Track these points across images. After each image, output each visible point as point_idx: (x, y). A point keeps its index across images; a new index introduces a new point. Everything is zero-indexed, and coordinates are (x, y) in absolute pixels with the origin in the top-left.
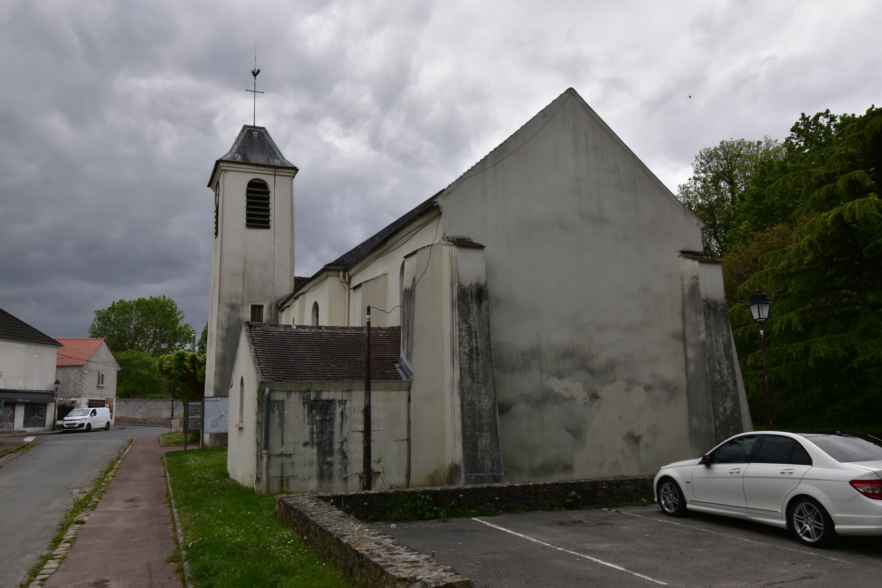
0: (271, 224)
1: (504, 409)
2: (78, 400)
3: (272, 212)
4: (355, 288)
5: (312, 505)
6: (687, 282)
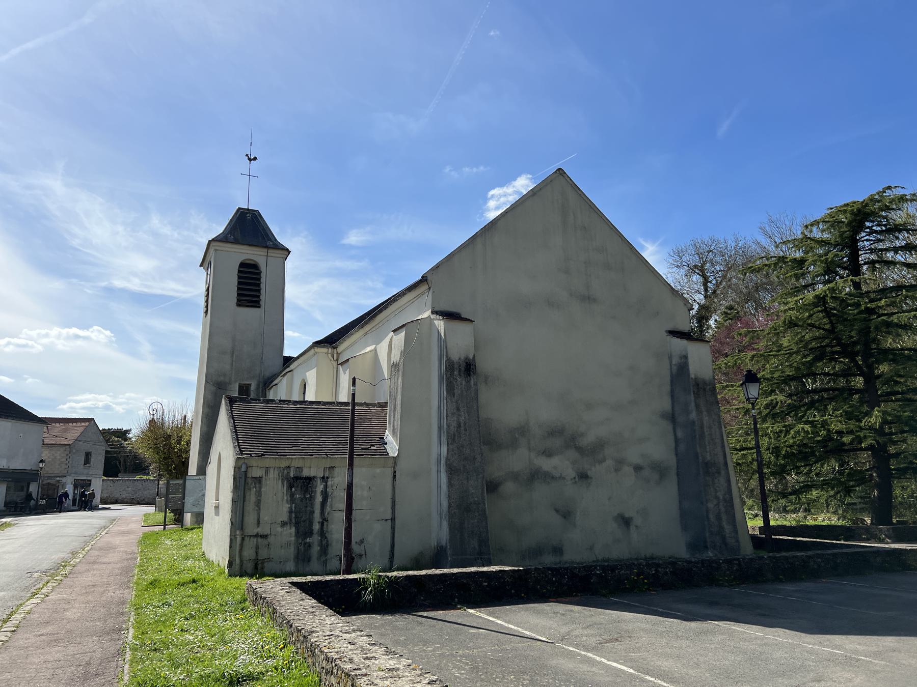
0: (262, 303)
1: (492, 487)
2: (64, 480)
3: (262, 292)
4: (341, 364)
5: (283, 593)
6: (675, 361)
